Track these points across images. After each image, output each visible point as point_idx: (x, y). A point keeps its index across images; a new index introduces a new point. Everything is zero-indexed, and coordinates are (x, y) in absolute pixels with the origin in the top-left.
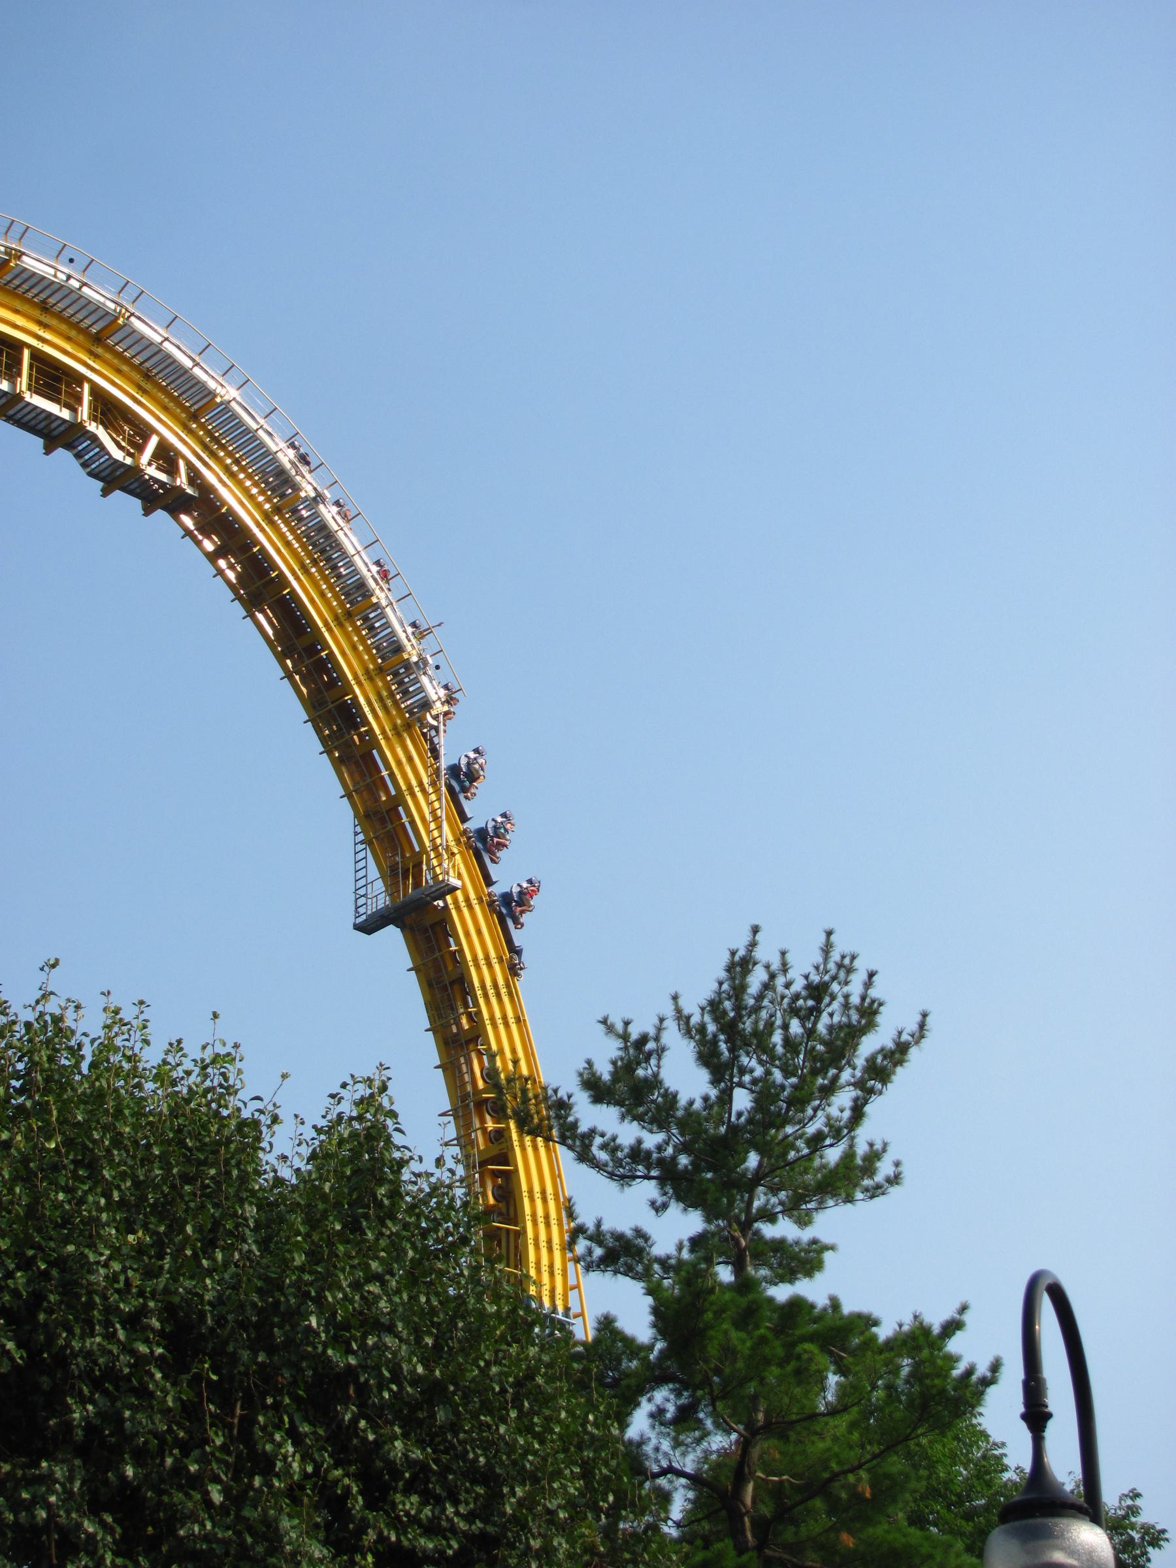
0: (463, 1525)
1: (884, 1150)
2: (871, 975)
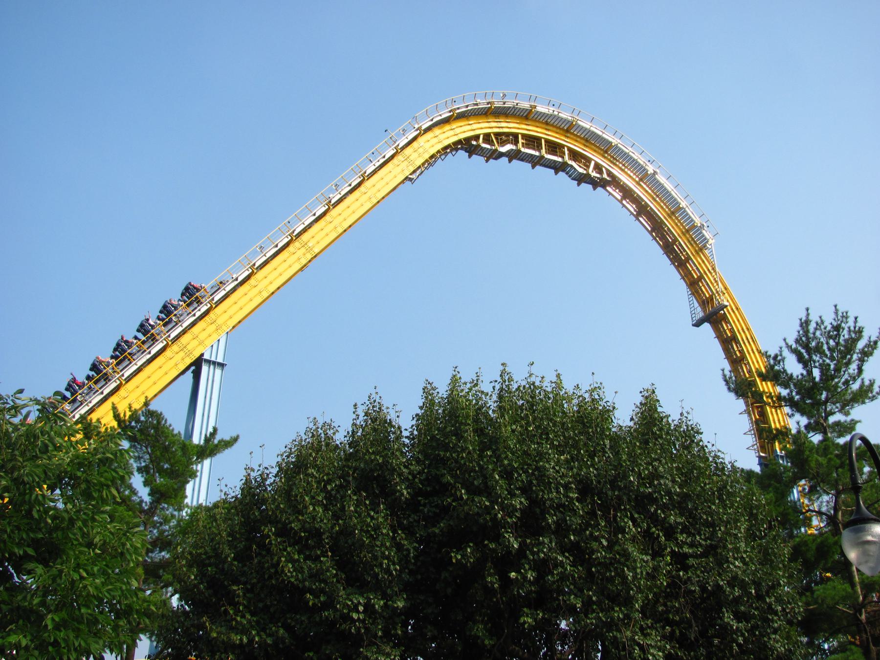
0: (703, 543)
1: (874, 382)
2: (856, 318)
